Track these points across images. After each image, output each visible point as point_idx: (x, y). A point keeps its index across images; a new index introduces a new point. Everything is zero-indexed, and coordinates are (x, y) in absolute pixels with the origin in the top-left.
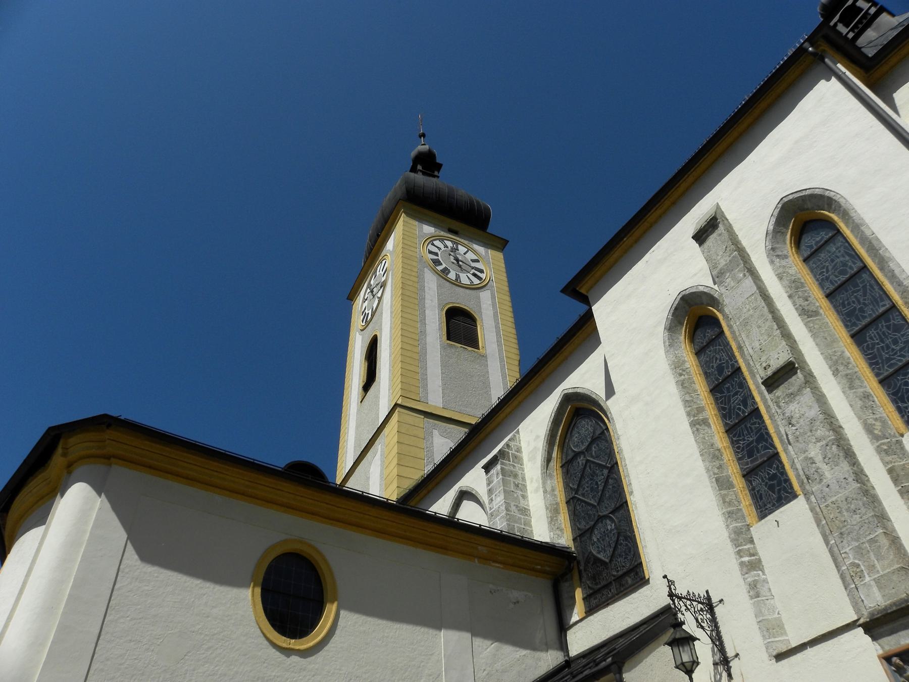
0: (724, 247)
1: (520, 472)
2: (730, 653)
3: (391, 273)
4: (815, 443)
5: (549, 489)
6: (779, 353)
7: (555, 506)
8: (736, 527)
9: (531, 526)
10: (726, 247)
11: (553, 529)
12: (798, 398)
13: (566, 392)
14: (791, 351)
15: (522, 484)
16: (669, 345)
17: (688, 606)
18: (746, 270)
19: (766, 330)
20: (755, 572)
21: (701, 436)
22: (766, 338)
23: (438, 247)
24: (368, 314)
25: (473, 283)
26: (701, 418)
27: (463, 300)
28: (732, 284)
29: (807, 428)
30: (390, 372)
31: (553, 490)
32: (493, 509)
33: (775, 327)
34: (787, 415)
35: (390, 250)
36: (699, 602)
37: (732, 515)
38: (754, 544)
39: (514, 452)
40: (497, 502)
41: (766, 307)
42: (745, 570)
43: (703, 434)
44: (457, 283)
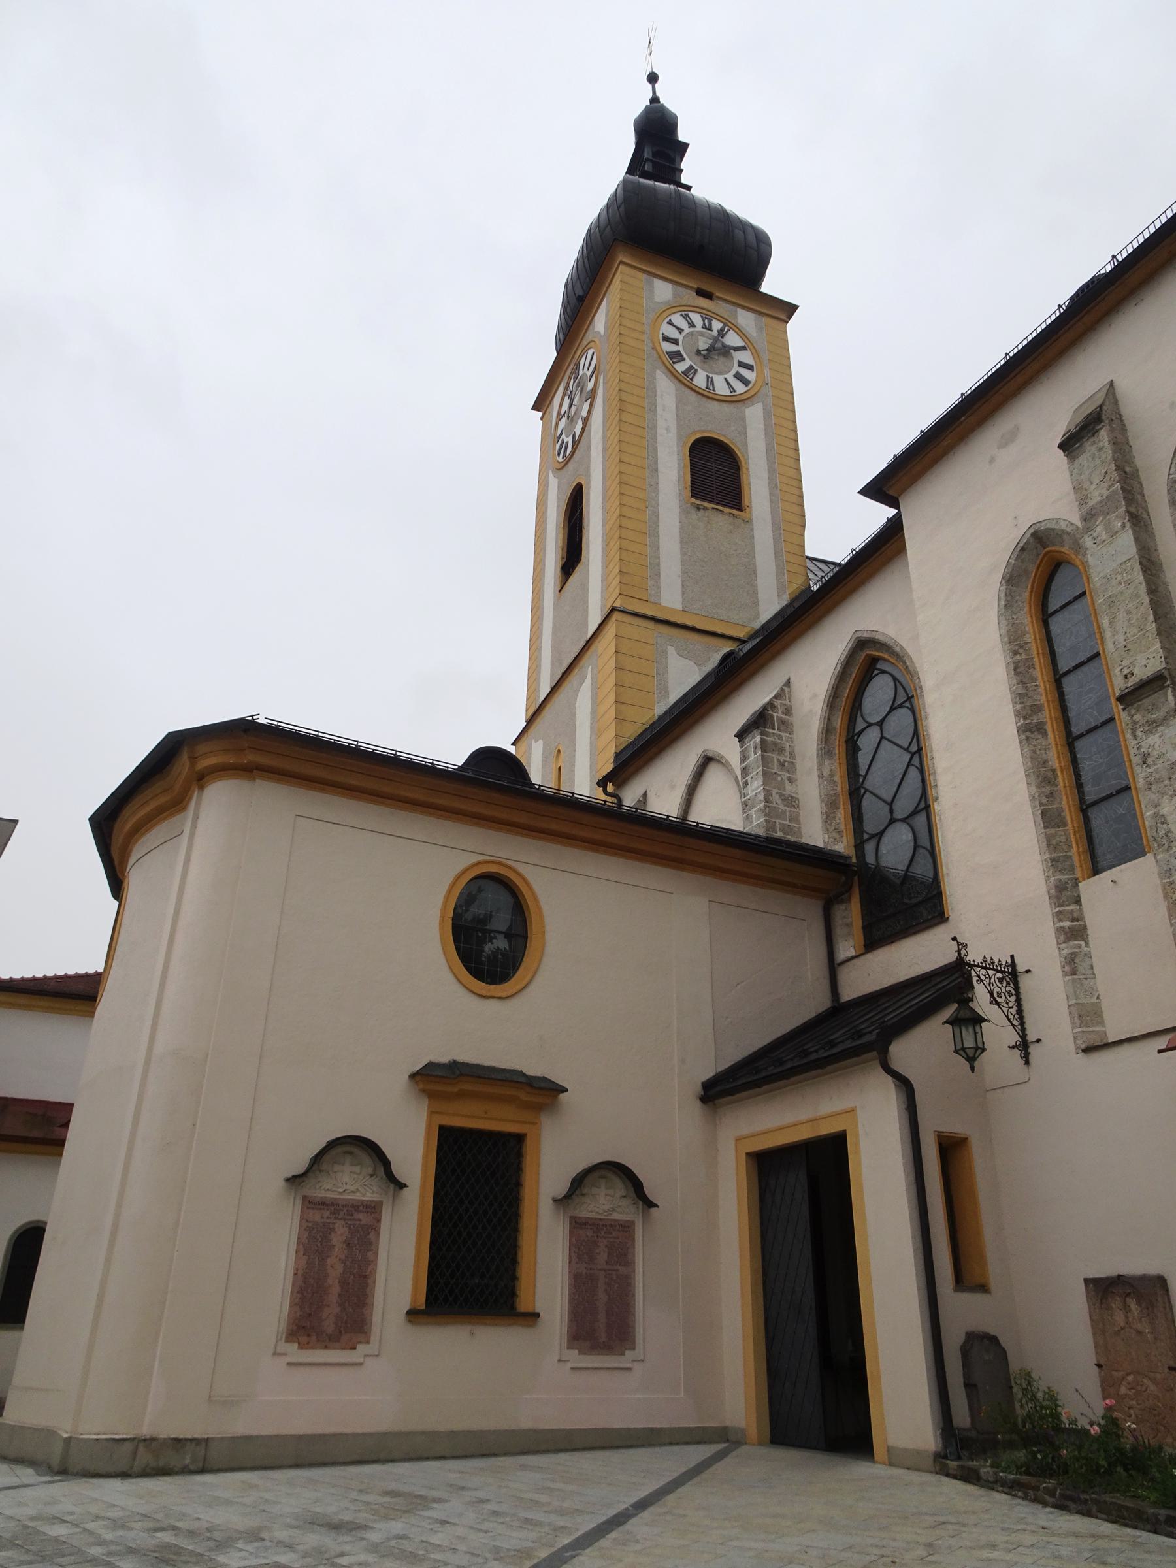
0: (1103, 471)
1: (788, 744)
2: (1031, 1037)
3: (590, 669)
4: (1171, 796)
5: (826, 772)
6: (1148, 658)
7: (834, 798)
8: (1060, 880)
9: (799, 822)
10: (1106, 473)
11: (828, 830)
12: (1161, 729)
13: (859, 635)
14: (1166, 658)
15: (789, 762)
16: (1005, 606)
17: (981, 976)
18: (1127, 518)
19: (1138, 619)
20: (1076, 942)
21: (1032, 748)
22: (1136, 631)
23: (678, 328)
24: (567, 443)
25: (735, 391)
26: (1035, 721)
27: (720, 429)
28: (1104, 537)
29: (1165, 774)
30: (603, 552)
31: (832, 775)
32: (748, 797)
33: (1151, 618)
34: (1142, 750)
35: (599, 333)
36: (998, 971)
37: (1057, 863)
38: (1081, 905)
39: (780, 715)
40: (753, 787)
41: (1144, 584)
42: (1062, 938)
43: (1035, 746)
44: (708, 394)
